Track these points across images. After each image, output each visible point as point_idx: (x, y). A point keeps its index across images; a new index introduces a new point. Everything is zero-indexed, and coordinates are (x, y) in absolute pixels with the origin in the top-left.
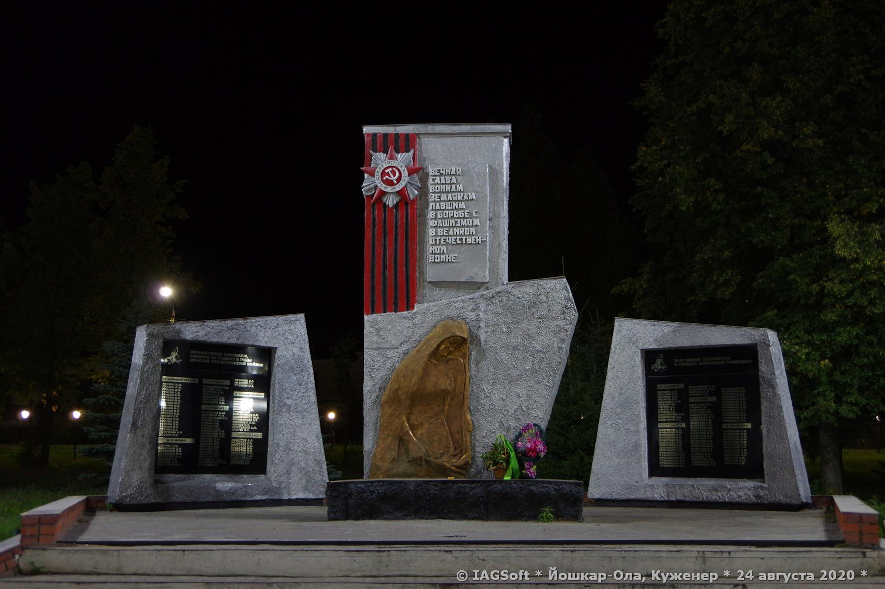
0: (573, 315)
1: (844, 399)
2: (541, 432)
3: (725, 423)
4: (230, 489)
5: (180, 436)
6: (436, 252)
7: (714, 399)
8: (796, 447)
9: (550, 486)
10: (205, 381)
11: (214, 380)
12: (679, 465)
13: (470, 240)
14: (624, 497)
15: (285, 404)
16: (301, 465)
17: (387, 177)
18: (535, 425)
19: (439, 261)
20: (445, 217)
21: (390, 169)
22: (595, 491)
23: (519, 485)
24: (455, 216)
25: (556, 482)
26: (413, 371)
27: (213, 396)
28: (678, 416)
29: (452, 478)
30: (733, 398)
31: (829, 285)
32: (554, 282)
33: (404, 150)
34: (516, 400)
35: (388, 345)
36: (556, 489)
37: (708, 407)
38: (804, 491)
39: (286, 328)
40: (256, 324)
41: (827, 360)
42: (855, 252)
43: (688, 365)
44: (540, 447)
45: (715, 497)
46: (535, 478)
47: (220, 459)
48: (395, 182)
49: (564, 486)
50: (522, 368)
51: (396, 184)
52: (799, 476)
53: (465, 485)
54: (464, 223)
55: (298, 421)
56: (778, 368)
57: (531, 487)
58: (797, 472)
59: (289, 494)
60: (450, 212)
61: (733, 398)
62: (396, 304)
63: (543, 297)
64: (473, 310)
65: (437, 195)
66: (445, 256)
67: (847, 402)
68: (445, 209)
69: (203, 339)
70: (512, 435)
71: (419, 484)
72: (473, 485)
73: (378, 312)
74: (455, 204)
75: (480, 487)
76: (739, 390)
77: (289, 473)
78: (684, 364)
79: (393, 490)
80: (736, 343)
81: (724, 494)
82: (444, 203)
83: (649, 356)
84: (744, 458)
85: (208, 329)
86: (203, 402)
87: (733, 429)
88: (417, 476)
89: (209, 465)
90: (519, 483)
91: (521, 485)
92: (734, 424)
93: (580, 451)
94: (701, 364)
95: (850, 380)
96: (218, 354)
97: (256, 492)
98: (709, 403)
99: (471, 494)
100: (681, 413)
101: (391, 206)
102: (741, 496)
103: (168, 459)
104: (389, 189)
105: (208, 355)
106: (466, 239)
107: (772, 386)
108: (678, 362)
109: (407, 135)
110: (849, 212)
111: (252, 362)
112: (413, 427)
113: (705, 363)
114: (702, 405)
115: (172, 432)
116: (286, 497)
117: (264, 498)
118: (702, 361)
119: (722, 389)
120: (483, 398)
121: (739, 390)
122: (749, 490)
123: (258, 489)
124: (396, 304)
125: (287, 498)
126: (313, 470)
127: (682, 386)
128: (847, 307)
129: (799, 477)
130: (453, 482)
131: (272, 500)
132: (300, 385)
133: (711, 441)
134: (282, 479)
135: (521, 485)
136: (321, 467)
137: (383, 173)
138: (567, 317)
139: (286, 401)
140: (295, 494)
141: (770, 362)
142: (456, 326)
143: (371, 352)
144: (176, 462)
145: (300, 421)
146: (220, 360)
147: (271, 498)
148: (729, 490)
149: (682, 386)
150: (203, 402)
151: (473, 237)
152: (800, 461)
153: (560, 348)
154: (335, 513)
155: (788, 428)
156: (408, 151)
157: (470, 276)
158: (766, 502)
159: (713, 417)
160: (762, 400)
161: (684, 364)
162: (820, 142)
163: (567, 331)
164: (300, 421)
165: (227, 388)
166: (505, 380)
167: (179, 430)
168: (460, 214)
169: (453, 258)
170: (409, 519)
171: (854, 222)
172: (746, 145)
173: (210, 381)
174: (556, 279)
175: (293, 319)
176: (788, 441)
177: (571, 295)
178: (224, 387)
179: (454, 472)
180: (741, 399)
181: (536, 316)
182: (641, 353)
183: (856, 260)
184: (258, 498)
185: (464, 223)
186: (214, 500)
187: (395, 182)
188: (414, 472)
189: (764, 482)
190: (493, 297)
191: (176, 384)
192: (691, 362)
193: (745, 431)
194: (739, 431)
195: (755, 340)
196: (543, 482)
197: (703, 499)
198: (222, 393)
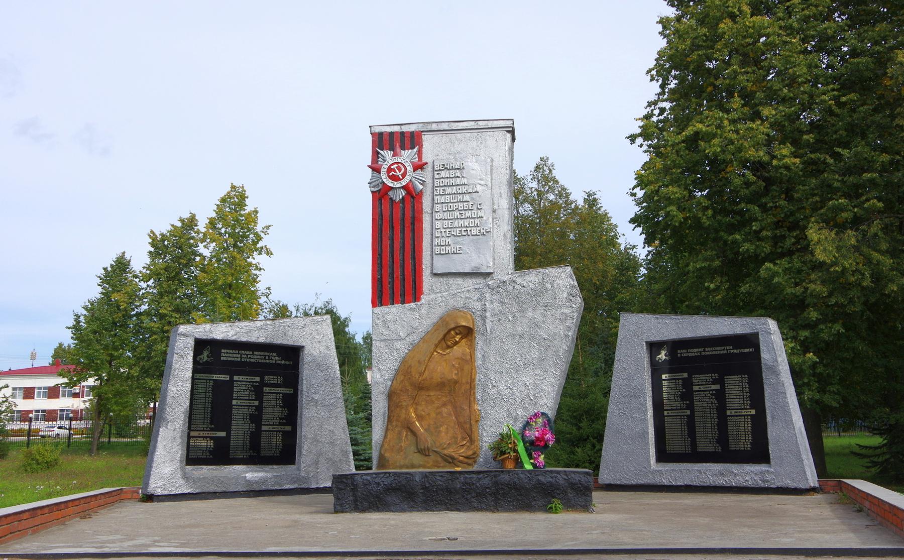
0: (578, 301)
1: (828, 389)
2: (549, 420)
3: (729, 409)
4: (260, 479)
5: (212, 430)
6: (442, 244)
7: (717, 387)
8: (801, 433)
9: (558, 475)
10: (236, 378)
11: (201, 375)
12: (686, 451)
13: (475, 231)
14: (633, 483)
15: (313, 399)
16: (328, 455)
17: (393, 173)
18: (543, 414)
19: (444, 252)
20: (449, 209)
21: (396, 165)
22: (605, 476)
23: (526, 475)
24: (460, 209)
25: (565, 471)
26: (419, 362)
27: (244, 392)
28: (683, 404)
29: (459, 469)
30: (736, 385)
31: (812, 286)
32: (559, 270)
33: (409, 146)
34: (523, 389)
35: (395, 337)
36: (565, 479)
37: (712, 395)
38: (812, 479)
39: (313, 327)
40: (284, 324)
41: (811, 354)
42: (834, 256)
43: (691, 355)
44: (548, 436)
45: (721, 481)
46: (543, 468)
47: (251, 451)
48: (401, 177)
49: (573, 475)
50: (528, 357)
51: (402, 179)
52: (806, 461)
53: (471, 476)
54: (468, 214)
55: (324, 414)
56: (780, 356)
57: (540, 478)
58: (804, 457)
59: (317, 483)
60: (454, 205)
61: (736, 385)
62: (403, 295)
63: (548, 286)
64: (479, 300)
65: (442, 188)
66: (450, 247)
67: (829, 391)
68: (450, 202)
69: (233, 338)
70: (520, 425)
71: (425, 476)
72: (481, 475)
73: (386, 304)
74: (460, 197)
75: (487, 477)
76: (742, 378)
77: (317, 463)
78: (687, 354)
79: (399, 482)
80: (738, 332)
81: (731, 478)
82: (449, 196)
83: (654, 347)
84: (749, 443)
85: (238, 329)
86: (234, 398)
87: (737, 416)
88: (424, 467)
89: (240, 457)
90: (527, 473)
91: (529, 475)
92: (738, 411)
93: (592, 439)
94: (703, 353)
95: (833, 372)
96: (248, 353)
97: (285, 481)
98: (712, 390)
99: (478, 485)
100: (686, 401)
101: (398, 200)
102: (747, 481)
103: (200, 451)
104: (397, 185)
105: (239, 353)
106: (470, 230)
107: (775, 372)
108: (683, 353)
109: (412, 133)
110: (827, 222)
111: (281, 360)
112: (420, 418)
113: (708, 353)
114: (706, 393)
115: (204, 426)
116: (314, 486)
117: (292, 487)
118: (704, 351)
119: (726, 377)
120: (491, 387)
121: (742, 378)
122: (756, 474)
123: (286, 479)
124: (403, 295)
125: (315, 487)
126: (340, 460)
127: (685, 375)
128: (828, 306)
129: (806, 462)
130: (460, 473)
131: (300, 488)
132: (327, 380)
133: (716, 427)
134: (310, 469)
135: (529, 475)
136: (348, 458)
137: (389, 170)
138: (574, 305)
139: (314, 396)
140: (323, 483)
141: (772, 350)
142: (462, 316)
143: (378, 344)
144: (208, 454)
145: (327, 414)
146: (250, 358)
147: (299, 487)
148: (736, 475)
149: (685, 375)
150: (234, 398)
151: (479, 229)
152: (805, 447)
153: (567, 336)
154: (341, 505)
155: (793, 413)
156: (413, 148)
157: (475, 267)
158: (773, 486)
159: (717, 405)
160: (765, 387)
161: (687, 354)
162: (797, 160)
163: (573, 319)
164: (327, 414)
165: (257, 384)
166: (512, 369)
167: (211, 423)
168: (465, 206)
169: (458, 249)
170: (415, 511)
171: (832, 230)
172: (730, 167)
173: (241, 378)
174: (561, 267)
175: (320, 320)
176: (794, 427)
177: (576, 283)
178: (255, 384)
179: (461, 462)
180: (744, 386)
181: (541, 304)
182: (647, 345)
183: (834, 264)
184: (287, 487)
185: (468, 214)
186: (245, 490)
187: (401, 177)
188: (421, 463)
189: (770, 467)
190: (498, 287)
191: (208, 381)
192: (694, 352)
193: (749, 417)
194: (743, 417)
195: (756, 329)
196: (551, 472)
197: (711, 484)
198: (252, 388)
